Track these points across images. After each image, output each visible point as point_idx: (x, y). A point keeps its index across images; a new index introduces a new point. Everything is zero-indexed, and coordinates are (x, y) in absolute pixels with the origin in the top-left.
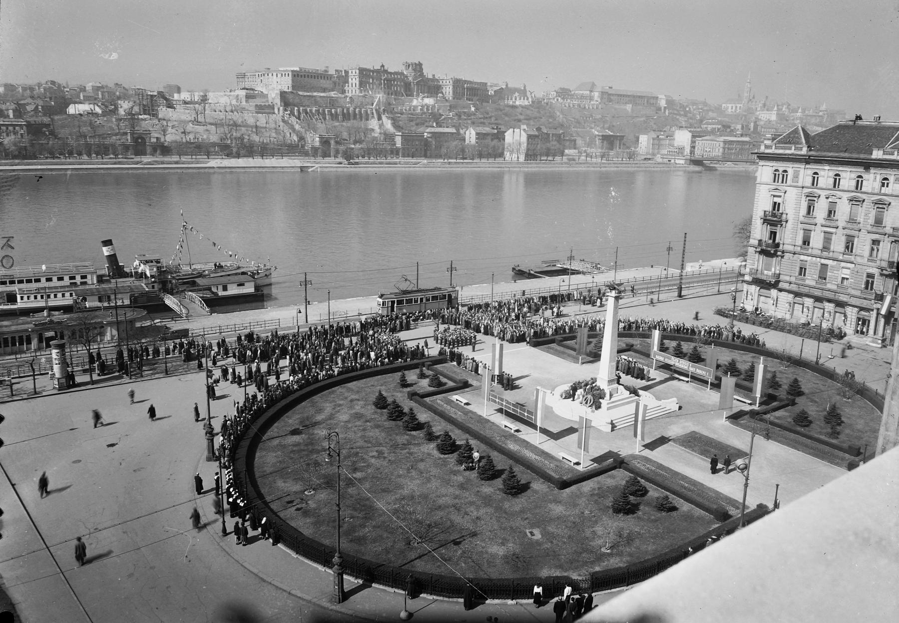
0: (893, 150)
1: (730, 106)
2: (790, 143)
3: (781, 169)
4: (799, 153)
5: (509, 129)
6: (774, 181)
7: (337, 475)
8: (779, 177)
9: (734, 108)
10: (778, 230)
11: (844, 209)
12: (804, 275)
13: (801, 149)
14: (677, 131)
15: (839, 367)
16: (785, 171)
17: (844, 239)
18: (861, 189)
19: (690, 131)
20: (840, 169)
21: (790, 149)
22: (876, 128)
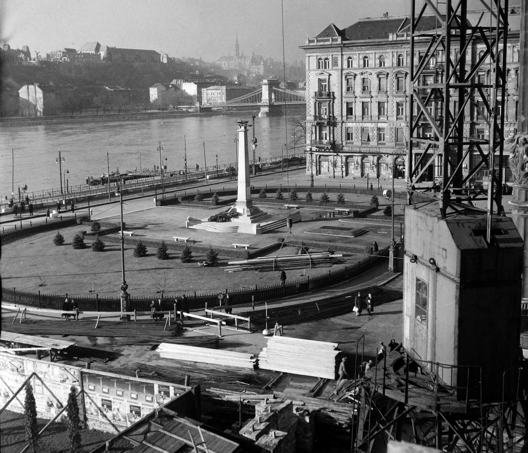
0: (403, 34)
1: (223, 62)
2: (328, 36)
3: (323, 57)
4: (335, 43)
5: (23, 86)
6: (319, 68)
7: (282, 64)
8: (322, 64)
9: (227, 64)
10: (36, 356)
11: (374, 82)
12: (352, 139)
13: (337, 40)
14: (184, 84)
15: (87, 406)
16: (327, 59)
17: (377, 105)
18: (384, 65)
19: (195, 83)
20: (367, 52)
21: (328, 40)
22: (386, 21)
